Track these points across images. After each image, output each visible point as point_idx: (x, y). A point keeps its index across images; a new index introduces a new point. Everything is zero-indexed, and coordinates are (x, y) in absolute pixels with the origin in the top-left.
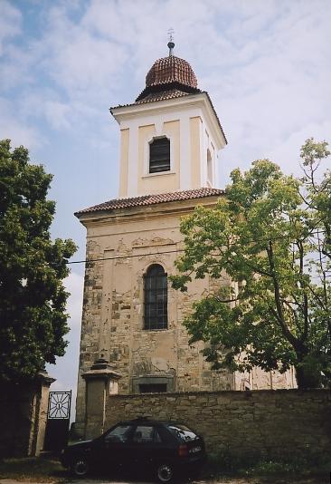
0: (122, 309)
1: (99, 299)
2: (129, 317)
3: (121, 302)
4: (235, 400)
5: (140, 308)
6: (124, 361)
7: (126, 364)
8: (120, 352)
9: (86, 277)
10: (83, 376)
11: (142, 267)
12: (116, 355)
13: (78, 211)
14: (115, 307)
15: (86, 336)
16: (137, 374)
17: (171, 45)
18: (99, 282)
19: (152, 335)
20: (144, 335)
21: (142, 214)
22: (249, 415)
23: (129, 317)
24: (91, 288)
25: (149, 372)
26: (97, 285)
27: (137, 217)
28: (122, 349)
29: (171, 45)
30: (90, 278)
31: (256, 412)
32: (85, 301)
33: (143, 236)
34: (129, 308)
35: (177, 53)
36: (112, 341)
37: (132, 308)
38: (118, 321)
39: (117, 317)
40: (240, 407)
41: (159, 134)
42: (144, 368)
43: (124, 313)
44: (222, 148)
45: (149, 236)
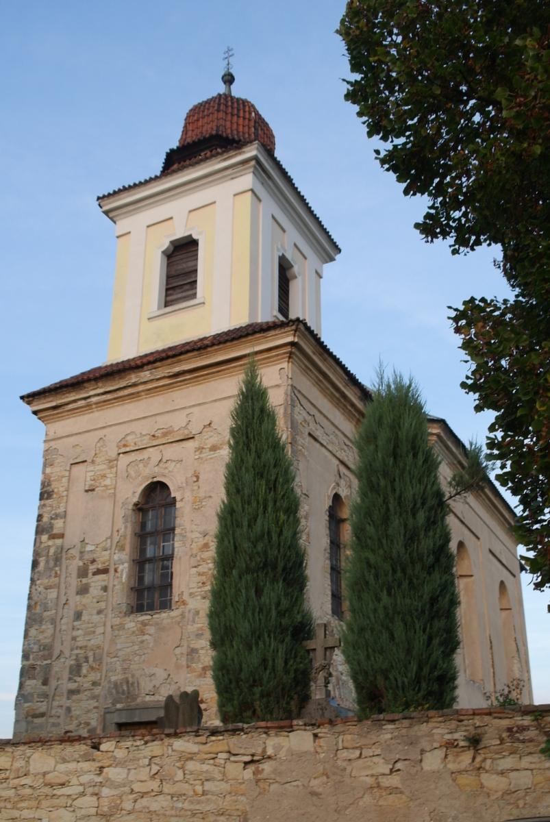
0: (94, 574)
1: (57, 560)
2: (105, 589)
3: (93, 561)
4: (64, 761)
5: (125, 569)
6: (93, 676)
7: (94, 684)
8: (86, 658)
9: (40, 517)
10: (360, 720)
11: (132, 492)
12: (79, 666)
13: (25, 393)
14: (83, 573)
15: (33, 632)
16: (114, 704)
17: (229, 79)
18: (58, 525)
19: (144, 624)
20: (132, 623)
21: (134, 385)
22: (89, 801)
23: (105, 589)
24: (44, 537)
25: (135, 699)
26: (55, 531)
27: (126, 392)
28: (90, 654)
29: (229, 79)
30: (45, 519)
31: (105, 791)
32: (35, 564)
33: (136, 428)
34: (105, 571)
35: (237, 91)
36: (74, 639)
37: (112, 571)
38: (86, 600)
39: (83, 590)
40: (74, 781)
41: (180, 233)
42: (125, 689)
43: (96, 582)
44: (332, 259)
45: (146, 428)
